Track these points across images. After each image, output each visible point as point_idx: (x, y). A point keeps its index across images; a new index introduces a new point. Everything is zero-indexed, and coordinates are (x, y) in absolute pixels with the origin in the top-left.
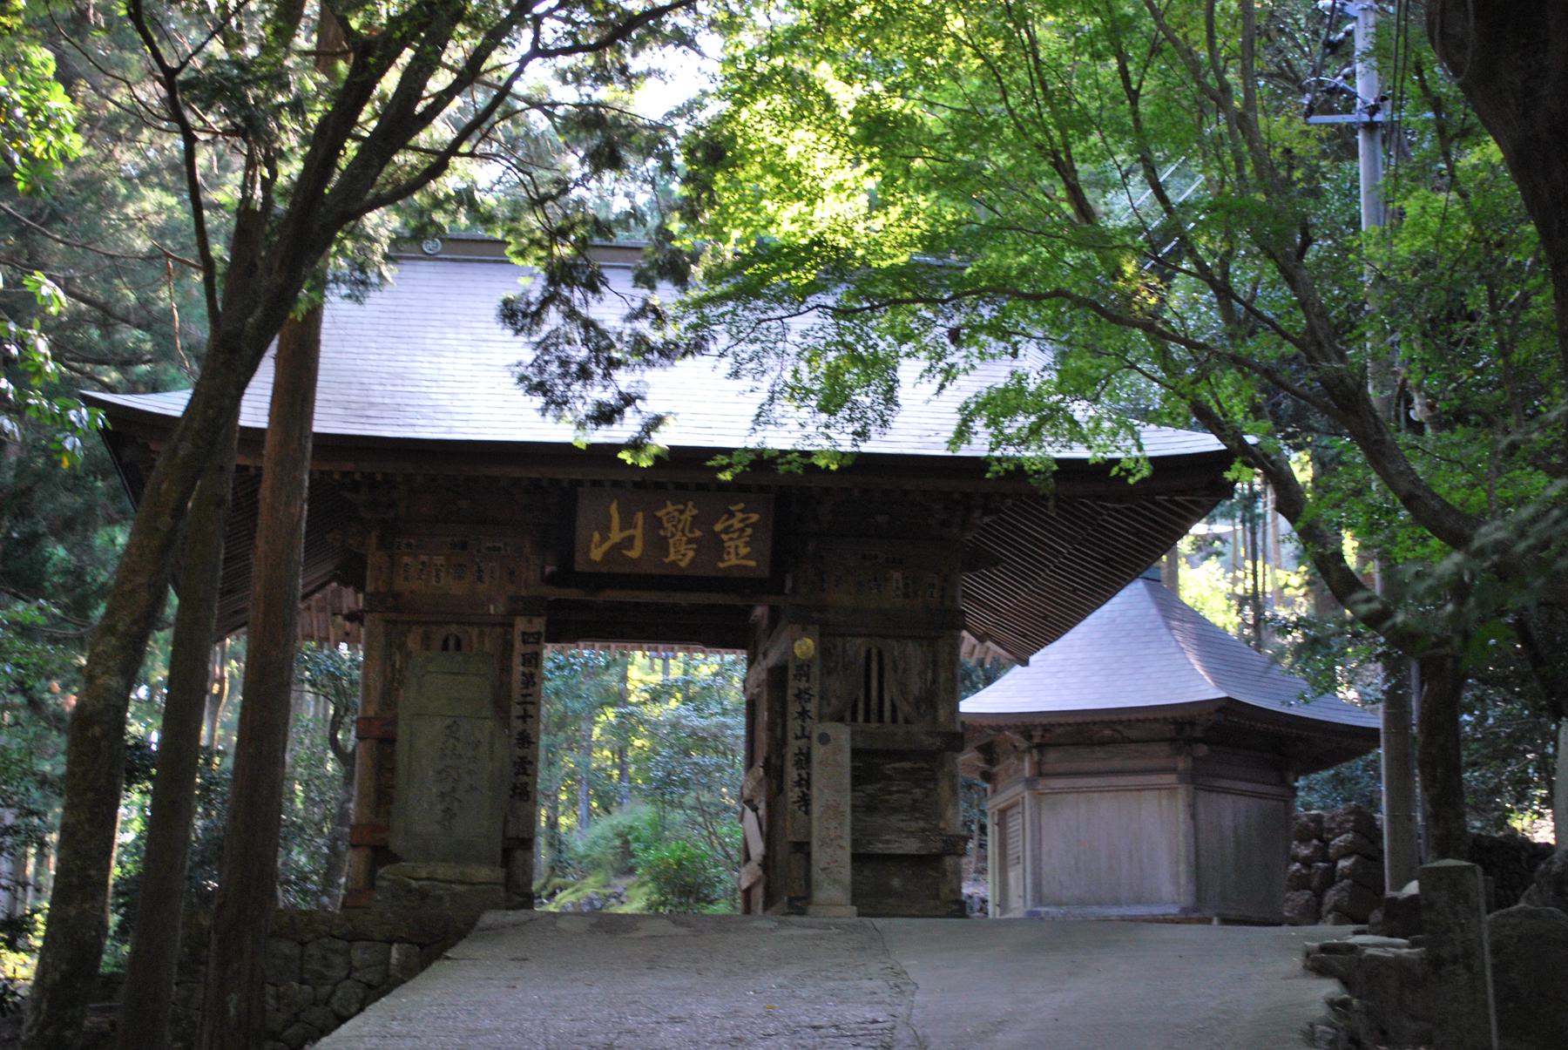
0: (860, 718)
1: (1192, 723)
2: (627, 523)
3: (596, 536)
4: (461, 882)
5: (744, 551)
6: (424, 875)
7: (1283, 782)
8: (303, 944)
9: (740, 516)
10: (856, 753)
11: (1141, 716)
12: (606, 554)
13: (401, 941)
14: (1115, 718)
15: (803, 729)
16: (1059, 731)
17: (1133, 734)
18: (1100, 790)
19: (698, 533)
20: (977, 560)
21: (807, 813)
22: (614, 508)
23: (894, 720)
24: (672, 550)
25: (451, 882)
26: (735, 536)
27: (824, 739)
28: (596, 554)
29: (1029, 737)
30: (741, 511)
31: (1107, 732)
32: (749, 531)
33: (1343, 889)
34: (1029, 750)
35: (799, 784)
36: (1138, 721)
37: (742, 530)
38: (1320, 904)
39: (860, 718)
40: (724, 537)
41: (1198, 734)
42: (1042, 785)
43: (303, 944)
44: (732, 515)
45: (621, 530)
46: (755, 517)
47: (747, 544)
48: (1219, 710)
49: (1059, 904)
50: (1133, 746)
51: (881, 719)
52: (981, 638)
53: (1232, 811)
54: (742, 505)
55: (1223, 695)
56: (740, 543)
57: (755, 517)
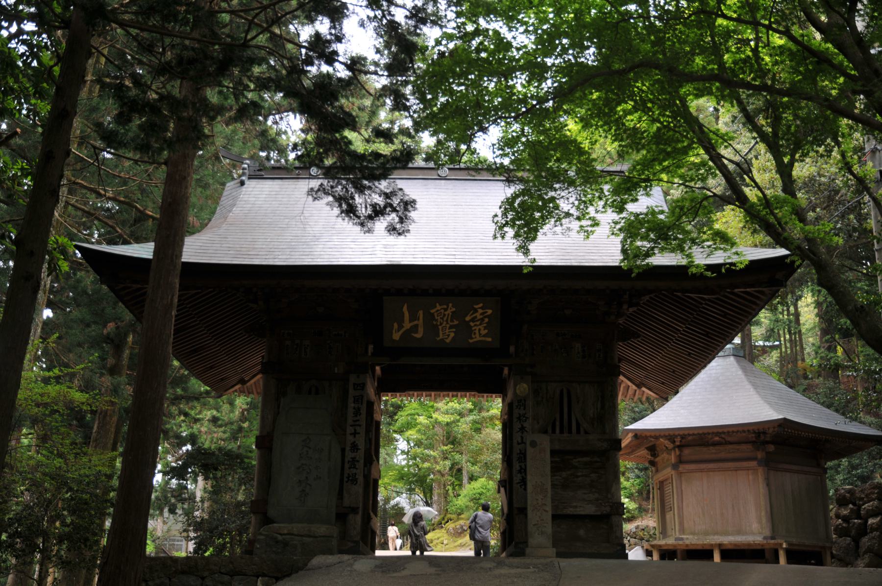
0: (558, 431)
1: (764, 433)
2: (413, 317)
3: (396, 325)
4: (309, 536)
5: (484, 332)
6: (286, 532)
7: (819, 465)
8: (203, 578)
9: (480, 311)
10: (553, 453)
11: (735, 429)
12: (401, 337)
13: (264, 575)
14: (720, 431)
15: (522, 438)
16: (690, 438)
17: (729, 439)
18: (713, 470)
19: (456, 322)
20: (627, 335)
21: (525, 489)
22: (405, 309)
23: (578, 432)
24: (441, 332)
25: (302, 536)
26: (478, 323)
27: (534, 444)
28: (396, 336)
29: (674, 442)
30: (482, 308)
31: (717, 438)
32: (487, 320)
33: (873, 538)
34: (674, 448)
35: (520, 472)
36: (733, 432)
37: (482, 320)
38: (857, 546)
39: (558, 431)
40: (472, 324)
41: (768, 439)
42: (682, 468)
43: (203, 578)
44: (476, 311)
45: (410, 321)
46: (490, 312)
47: (485, 328)
48: (780, 426)
49: (693, 534)
50: (731, 446)
51: (570, 432)
52: (639, 386)
53: (792, 481)
54: (481, 305)
55: (781, 417)
56: (481, 327)
57: (490, 312)
